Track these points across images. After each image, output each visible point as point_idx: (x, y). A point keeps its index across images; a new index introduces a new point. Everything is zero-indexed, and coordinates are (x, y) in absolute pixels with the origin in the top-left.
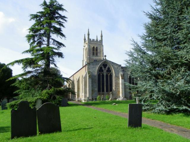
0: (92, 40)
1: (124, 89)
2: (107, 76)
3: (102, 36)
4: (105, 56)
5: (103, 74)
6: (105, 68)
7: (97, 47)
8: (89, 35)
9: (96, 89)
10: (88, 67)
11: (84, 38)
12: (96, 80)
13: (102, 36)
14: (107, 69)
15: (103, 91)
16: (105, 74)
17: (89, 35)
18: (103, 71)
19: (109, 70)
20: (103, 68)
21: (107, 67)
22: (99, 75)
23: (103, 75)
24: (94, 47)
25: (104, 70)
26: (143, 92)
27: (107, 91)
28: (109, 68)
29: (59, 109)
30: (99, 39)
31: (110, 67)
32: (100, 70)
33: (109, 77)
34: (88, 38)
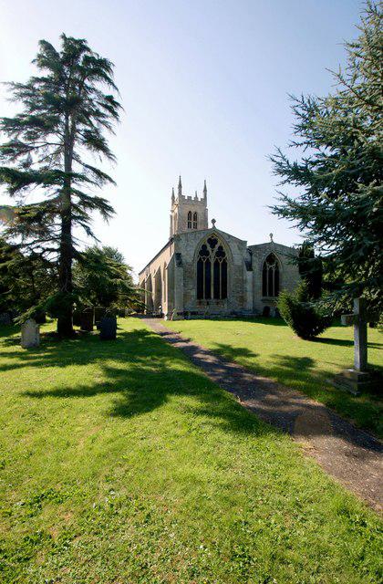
2: (216, 264)
3: (205, 190)
4: (214, 221)
6: (213, 246)
8: (180, 186)
9: (194, 293)
13: (205, 190)
15: (208, 296)
17: (180, 186)
19: (221, 253)
20: (209, 248)
21: (217, 246)
22: (200, 263)
27: (217, 296)
32: (204, 252)
33: (222, 267)
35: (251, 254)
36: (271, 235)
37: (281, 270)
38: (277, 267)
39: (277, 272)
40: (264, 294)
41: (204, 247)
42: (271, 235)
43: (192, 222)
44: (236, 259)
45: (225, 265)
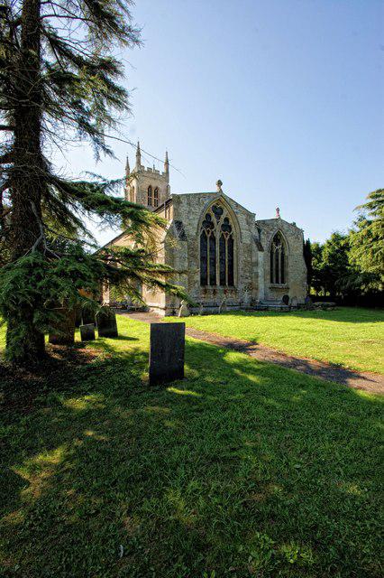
0: (146, 169)
1: (259, 312)
2: (222, 239)
5: (212, 233)
7: (157, 188)
10: (175, 209)
11: (126, 165)
12: (196, 250)
14: (222, 221)
16: (218, 235)
17: (139, 154)
18: (211, 225)
19: (227, 227)
20: (214, 219)
21: (223, 217)
22: (204, 237)
23: (213, 239)
24: (150, 187)
25: (215, 222)
26: (143, 386)
28: (227, 220)
29: (114, 322)
30: (162, 169)
31: (230, 217)
32: (208, 223)
34: (139, 162)
35: (259, 231)
36: (220, 183)
37: (287, 253)
38: (282, 249)
39: (283, 255)
40: (272, 282)
41: (208, 216)
42: (220, 183)
43: (153, 197)
44: (244, 236)
45: (231, 241)
